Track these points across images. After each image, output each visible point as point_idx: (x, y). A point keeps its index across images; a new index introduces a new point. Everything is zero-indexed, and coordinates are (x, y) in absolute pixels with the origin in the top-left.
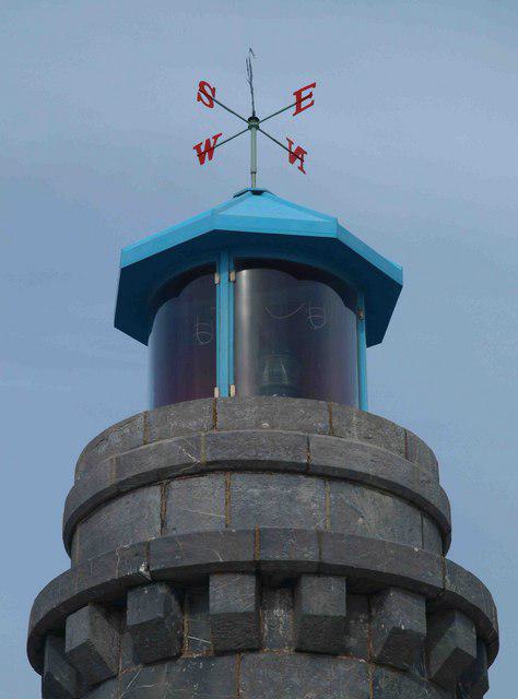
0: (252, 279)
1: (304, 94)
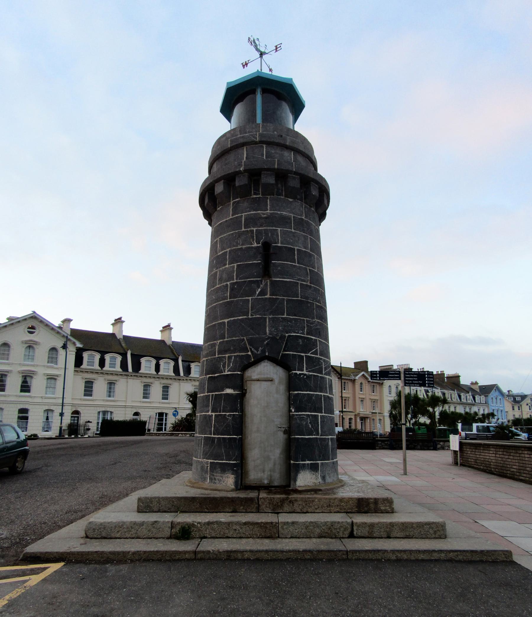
1: (278, 46)
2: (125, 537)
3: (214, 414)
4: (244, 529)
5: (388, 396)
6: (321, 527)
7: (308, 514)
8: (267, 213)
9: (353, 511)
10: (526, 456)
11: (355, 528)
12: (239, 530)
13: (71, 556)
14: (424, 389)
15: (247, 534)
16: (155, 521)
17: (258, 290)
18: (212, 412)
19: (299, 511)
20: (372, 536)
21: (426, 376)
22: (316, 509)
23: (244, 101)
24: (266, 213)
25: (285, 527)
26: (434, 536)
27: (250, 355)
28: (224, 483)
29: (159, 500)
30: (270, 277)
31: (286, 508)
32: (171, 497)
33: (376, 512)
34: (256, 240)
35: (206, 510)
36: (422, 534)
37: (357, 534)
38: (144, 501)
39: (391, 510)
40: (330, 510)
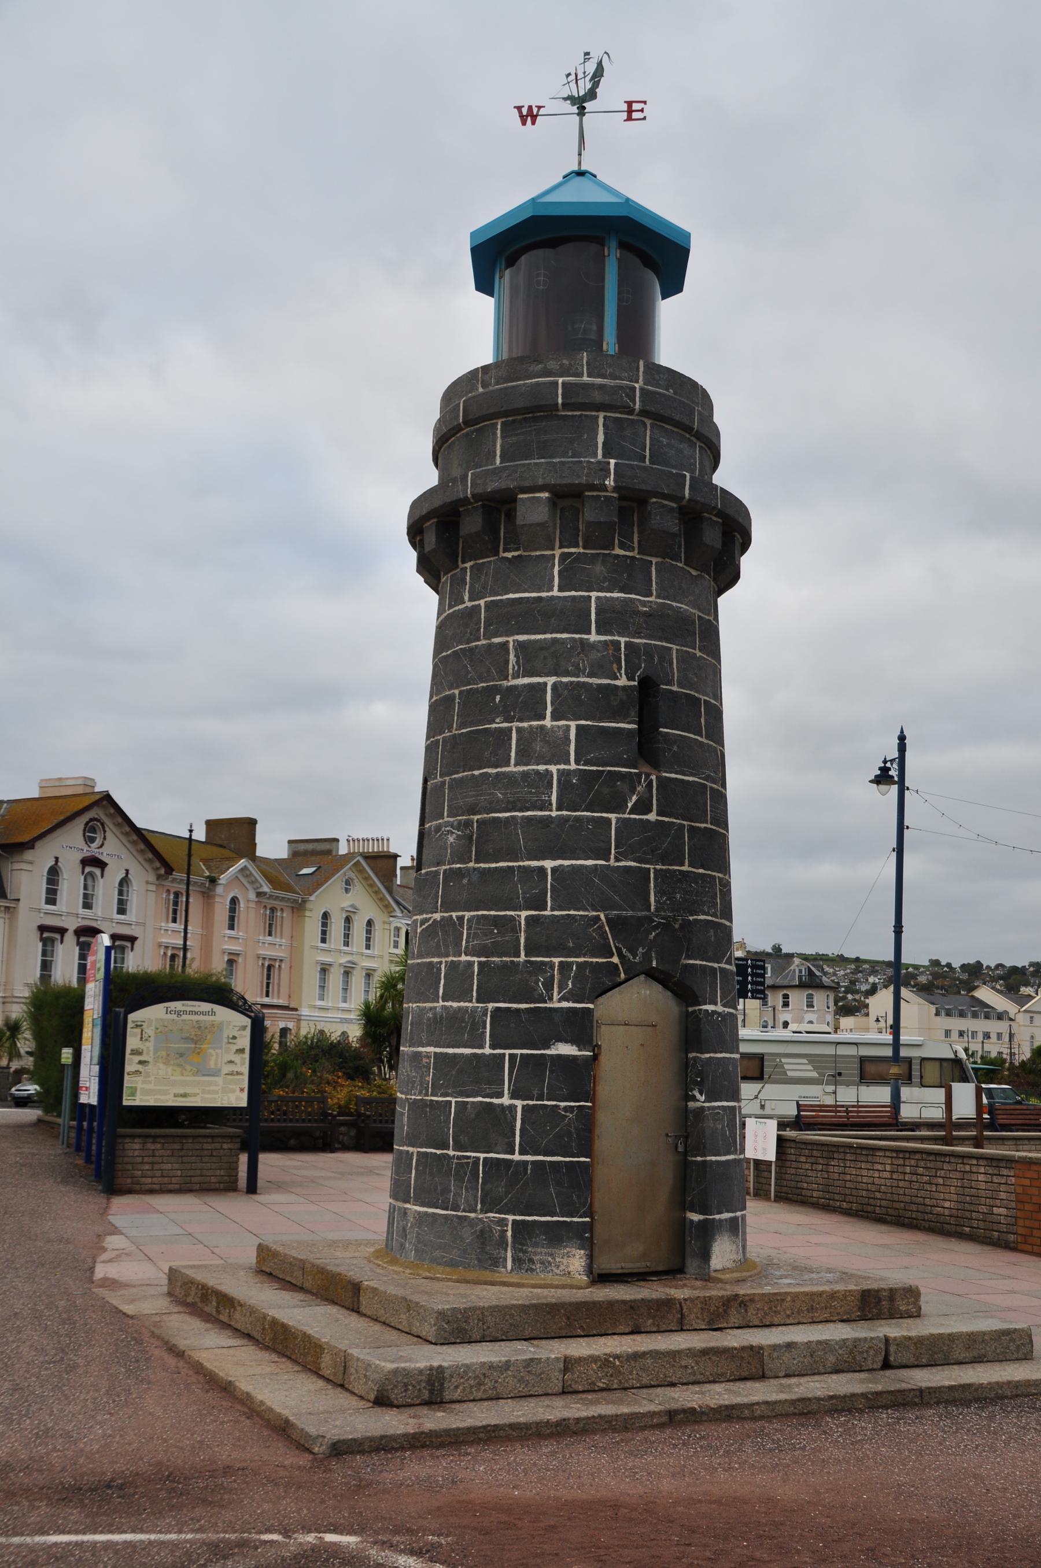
1: (635, 106)
2: (472, 1398)
3: (519, 1103)
4: (701, 1364)
5: (317, 948)
6: (836, 1350)
7: (774, 1329)
8: (651, 602)
9: (853, 1317)
10: (981, 1178)
11: (892, 1349)
12: (692, 1367)
13: (434, 1440)
15: (708, 1373)
16: (530, 1359)
17: (631, 799)
18: (513, 1096)
19: (757, 1323)
20: (921, 1363)
21: (749, 970)
22: (788, 1316)
24: (648, 601)
25: (775, 1355)
26: (1015, 1356)
27: (617, 965)
28: (558, 1268)
29: (482, 1313)
30: (656, 766)
31: (734, 1319)
32: (507, 1307)
33: (891, 1317)
34: (625, 669)
35: (580, 1332)
36: (998, 1354)
37: (895, 1360)
38: (450, 1319)
40: (812, 1318)
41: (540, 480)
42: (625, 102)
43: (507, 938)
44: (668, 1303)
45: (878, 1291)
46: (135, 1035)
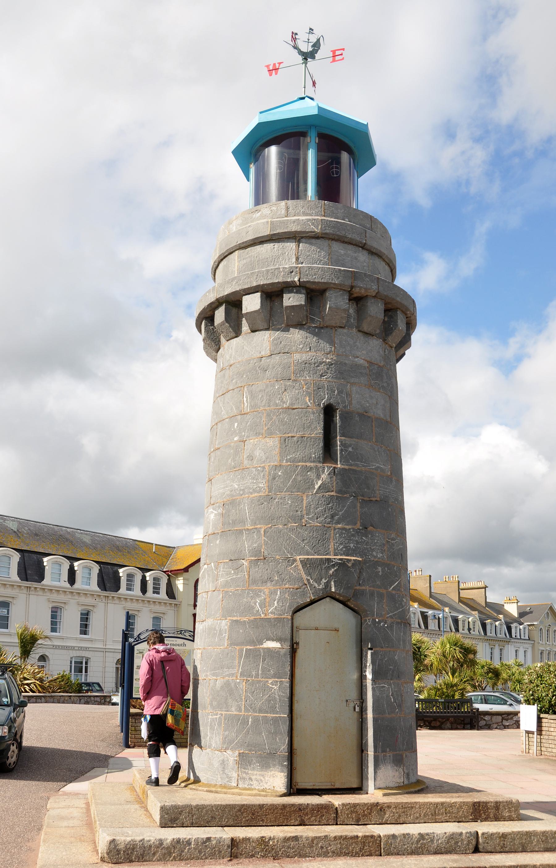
0: (281, 156)
1: (338, 53)
14: (421, 612)
23: (282, 144)
39: (516, 817)
41: (254, 283)
42: (331, 51)
43: (239, 576)
44: (327, 807)
45: (486, 803)
46: (139, 658)
